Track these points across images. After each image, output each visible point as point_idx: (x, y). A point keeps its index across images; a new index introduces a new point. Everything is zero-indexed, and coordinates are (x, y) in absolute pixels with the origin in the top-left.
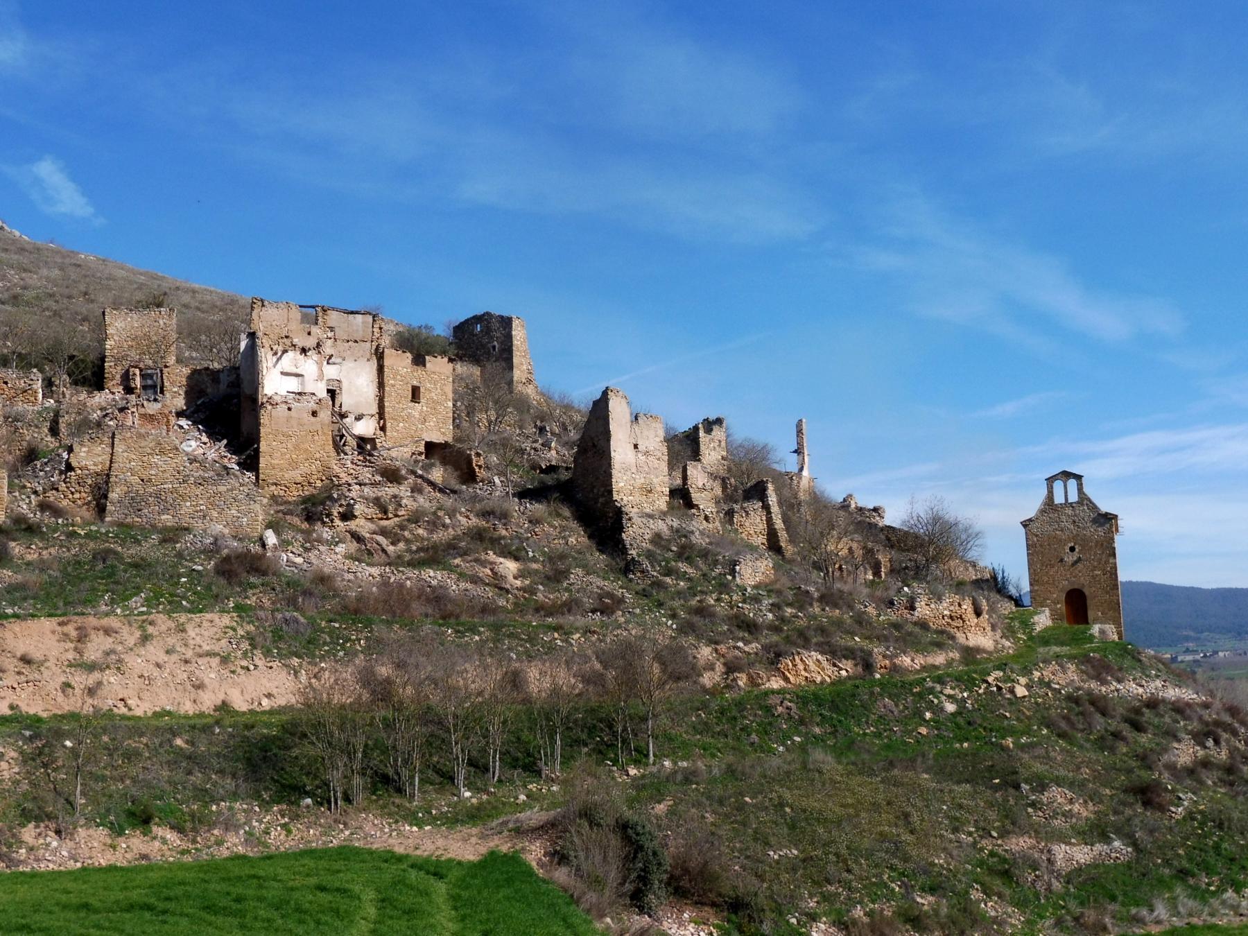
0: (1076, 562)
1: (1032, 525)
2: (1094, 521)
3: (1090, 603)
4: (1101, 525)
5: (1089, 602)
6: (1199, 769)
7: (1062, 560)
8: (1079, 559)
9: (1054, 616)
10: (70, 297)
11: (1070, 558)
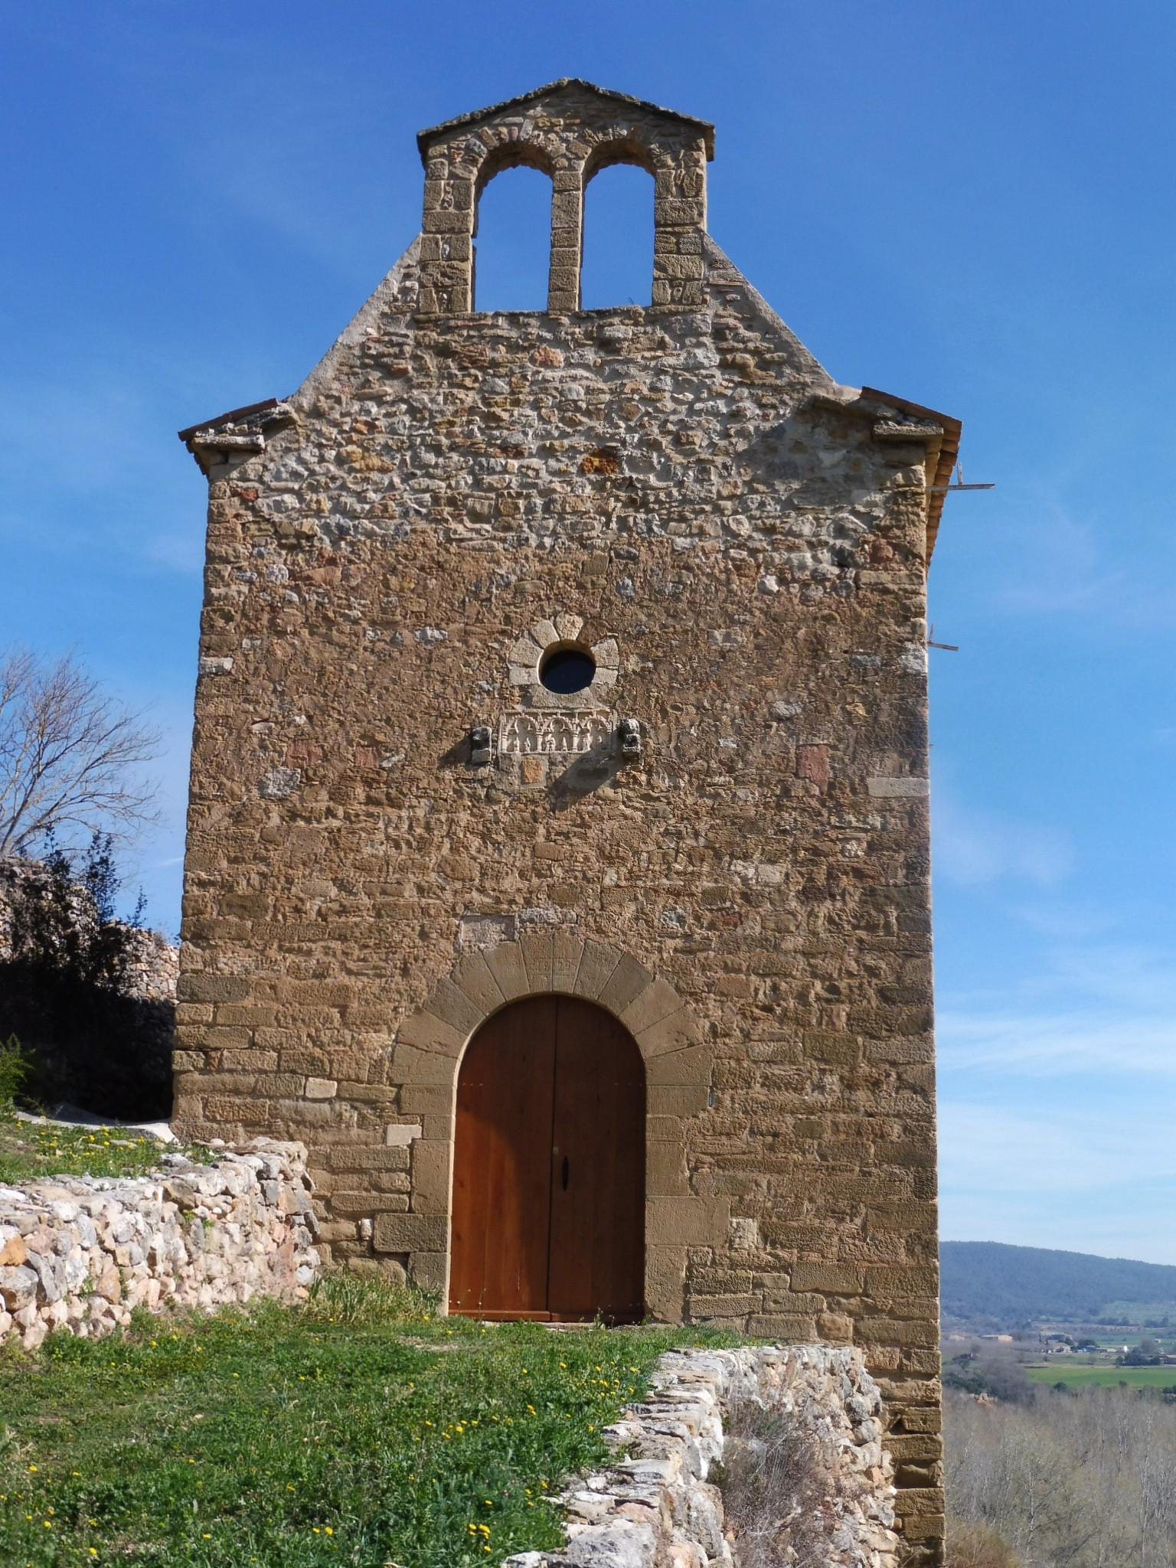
0: (574, 784)
1: (275, 461)
2: (768, 457)
3: (670, 1126)
4: (823, 492)
5: (662, 1117)
6: (848, 1492)
7: (470, 750)
8: (618, 753)
9: (357, 1220)
10: (152, 1260)
11: (542, 740)
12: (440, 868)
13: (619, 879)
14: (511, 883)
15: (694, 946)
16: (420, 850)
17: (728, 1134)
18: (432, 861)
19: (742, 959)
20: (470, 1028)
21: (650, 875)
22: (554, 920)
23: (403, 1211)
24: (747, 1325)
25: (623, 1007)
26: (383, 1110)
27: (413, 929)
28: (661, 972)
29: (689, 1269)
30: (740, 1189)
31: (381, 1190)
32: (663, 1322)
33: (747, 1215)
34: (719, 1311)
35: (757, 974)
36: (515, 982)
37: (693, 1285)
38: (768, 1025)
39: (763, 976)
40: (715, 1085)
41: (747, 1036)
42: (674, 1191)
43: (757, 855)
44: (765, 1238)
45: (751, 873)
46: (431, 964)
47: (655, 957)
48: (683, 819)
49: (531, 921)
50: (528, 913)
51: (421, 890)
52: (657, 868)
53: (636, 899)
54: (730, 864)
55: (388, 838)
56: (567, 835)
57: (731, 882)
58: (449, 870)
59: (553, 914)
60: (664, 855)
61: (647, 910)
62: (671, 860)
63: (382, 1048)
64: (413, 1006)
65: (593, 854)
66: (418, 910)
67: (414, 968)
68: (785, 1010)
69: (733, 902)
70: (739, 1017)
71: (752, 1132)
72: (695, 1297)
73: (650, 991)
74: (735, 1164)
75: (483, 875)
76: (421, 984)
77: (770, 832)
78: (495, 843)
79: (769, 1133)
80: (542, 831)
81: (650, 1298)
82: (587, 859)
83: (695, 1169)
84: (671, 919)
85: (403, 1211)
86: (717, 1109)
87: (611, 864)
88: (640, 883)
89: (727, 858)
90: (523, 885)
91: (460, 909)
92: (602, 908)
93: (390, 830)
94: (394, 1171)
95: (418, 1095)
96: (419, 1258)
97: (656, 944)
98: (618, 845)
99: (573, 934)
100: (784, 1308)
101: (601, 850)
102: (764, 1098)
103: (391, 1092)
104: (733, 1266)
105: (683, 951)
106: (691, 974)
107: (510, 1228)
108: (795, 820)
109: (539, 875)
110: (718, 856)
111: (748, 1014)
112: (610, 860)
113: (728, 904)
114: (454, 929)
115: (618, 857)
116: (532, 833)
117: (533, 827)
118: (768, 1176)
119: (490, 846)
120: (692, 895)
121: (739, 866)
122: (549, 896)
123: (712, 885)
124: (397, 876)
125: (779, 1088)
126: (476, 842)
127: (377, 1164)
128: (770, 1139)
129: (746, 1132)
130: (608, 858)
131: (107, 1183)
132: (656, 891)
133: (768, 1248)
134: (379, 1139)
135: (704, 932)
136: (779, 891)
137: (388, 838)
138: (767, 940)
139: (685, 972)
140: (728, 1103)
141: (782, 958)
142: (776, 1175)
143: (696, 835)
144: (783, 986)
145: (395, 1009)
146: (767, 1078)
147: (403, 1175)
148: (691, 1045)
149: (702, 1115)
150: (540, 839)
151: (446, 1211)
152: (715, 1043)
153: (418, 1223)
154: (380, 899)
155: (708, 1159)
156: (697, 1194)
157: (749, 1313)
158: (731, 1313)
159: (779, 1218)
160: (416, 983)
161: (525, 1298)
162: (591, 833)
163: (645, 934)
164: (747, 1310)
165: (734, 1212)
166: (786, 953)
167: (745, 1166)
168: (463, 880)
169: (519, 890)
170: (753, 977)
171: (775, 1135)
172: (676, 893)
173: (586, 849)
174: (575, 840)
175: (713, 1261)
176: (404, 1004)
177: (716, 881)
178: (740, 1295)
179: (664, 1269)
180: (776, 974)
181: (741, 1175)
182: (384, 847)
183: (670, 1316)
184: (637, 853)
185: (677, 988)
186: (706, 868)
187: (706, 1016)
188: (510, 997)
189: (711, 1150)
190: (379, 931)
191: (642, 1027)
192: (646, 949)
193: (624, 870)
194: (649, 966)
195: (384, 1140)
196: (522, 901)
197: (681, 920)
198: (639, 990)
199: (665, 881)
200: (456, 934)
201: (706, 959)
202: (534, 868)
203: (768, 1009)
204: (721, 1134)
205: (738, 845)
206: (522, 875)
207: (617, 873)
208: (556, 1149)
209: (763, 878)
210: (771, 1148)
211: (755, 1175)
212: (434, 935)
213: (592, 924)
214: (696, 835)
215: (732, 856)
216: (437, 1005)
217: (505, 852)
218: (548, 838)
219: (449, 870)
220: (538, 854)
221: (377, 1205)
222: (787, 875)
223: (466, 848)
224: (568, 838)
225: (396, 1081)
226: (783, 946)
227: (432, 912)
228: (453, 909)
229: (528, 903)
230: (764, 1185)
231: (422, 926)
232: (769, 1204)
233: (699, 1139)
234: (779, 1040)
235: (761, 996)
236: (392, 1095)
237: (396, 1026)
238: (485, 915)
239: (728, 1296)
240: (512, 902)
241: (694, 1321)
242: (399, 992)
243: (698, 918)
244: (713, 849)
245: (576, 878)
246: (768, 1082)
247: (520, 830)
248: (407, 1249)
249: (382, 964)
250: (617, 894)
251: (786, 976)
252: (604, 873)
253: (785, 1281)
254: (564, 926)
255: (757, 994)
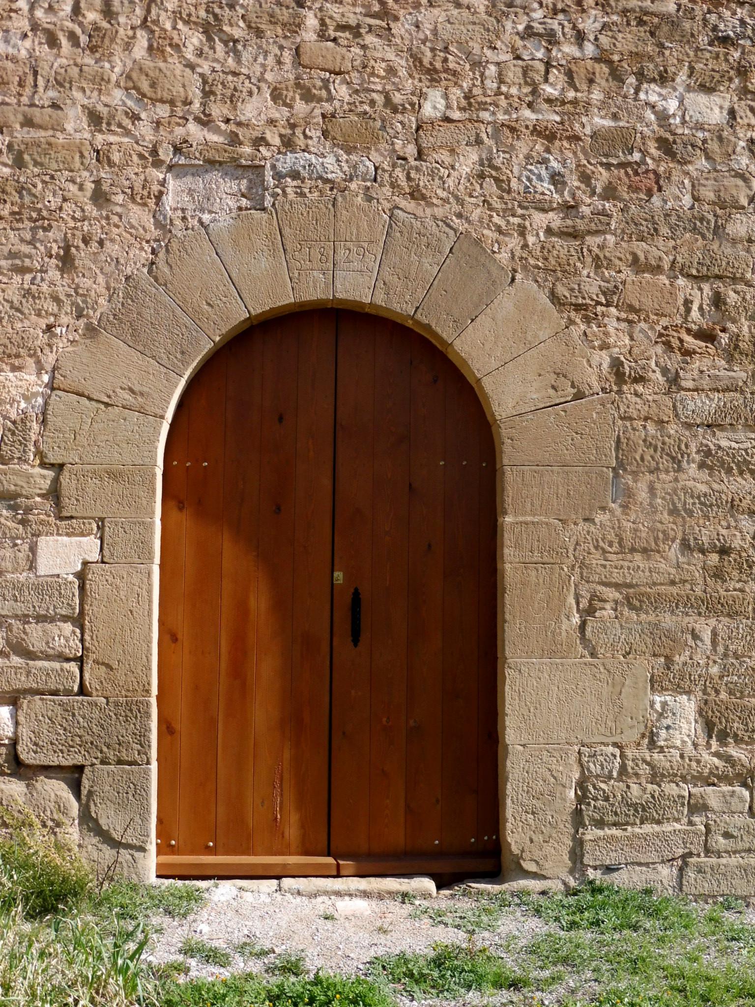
12: (129, 83)
13: (448, 107)
14: (255, 109)
15: (581, 225)
16: (93, 49)
17: (645, 551)
18: (116, 68)
19: (655, 250)
20: (185, 364)
21: (503, 102)
22: (336, 175)
23: (68, 693)
24: (681, 876)
25: (460, 328)
26: (28, 510)
27: (81, 188)
28: (525, 268)
29: (581, 784)
30: (665, 647)
31: (29, 655)
32: (535, 876)
33: (679, 690)
34: (634, 856)
35: (689, 276)
36: (268, 283)
37: (588, 813)
38: (707, 364)
39: (698, 279)
40: (621, 464)
41: (674, 381)
42: (553, 650)
43: (682, 77)
44: (709, 727)
45: (672, 105)
46: (113, 249)
47: (514, 242)
48: (555, 12)
49: (295, 175)
50: (287, 162)
51: (95, 119)
52: (514, 91)
53: (479, 142)
54: (637, 90)
55: (35, 27)
56: (356, 31)
57: (641, 118)
58: (144, 88)
59: (332, 165)
60: (525, 71)
61: (498, 162)
62: (538, 78)
63: (26, 398)
64: (82, 322)
65: (401, 64)
66: (90, 158)
67: (82, 256)
68: (736, 339)
69: (644, 153)
70: (659, 349)
71: (685, 546)
72: (591, 834)
73: (506, 302)
74: (657, 602)
75: (207, 94)
76: (94, 284)
77: (703, 40)
78: (231, 42)
79: (713, 549)
80: (312, 21)
81: (516, 835)
82: (391, 71)
83: (590, 611)
84: (540, 178)
85: (68, 693)
86: (625, 507)
87: (434, 81)
88: (485, 116)
89: (632, 80)
90: (280, 114)
91: (166, 154)
92: (420, 156)
93: (39, 13)
94: (52, 620)
95: (92, 484)
96: (101, 778)
97: (516, 220)
98: (446, 49)
99: (369, 199)
100: (740, 846)
101: (417, 59)
102: (703, 488)
103: (43, 478)
104: (656, 777)
105: (563, 234)
106: (576, 273)
107: (263, 712)
108: (743, 22)
109: (308, 97)
110: (616, 75)
111: (675, 343)
112: (432, 75)
113: (637, 156)
114: (155, 188)
115: (447, 70)
116: (295, 26)
117: (297, 15)
118: (713, 622)
119: (219, 47)
120: (576, 138)
121: (652, 93)
122: (325, 134)
123: (608, 123)
124: (51, 93)
125: (729, 471)
126: (195, 39)
127: (20, 608)
128: (714, 558)
129: (676, 545)
130: (428, 71)
131: (496, 414)
132: (513, 130)
133: (714, 743)
134: (23, 563)
135: (599, 204)
136: (720, 138)
137: (35, 27)
138: (702, 220)
139: (567, 271)
140: (643, 495)
141: (728, 251)
142: (725, 620)
143: (580, 37)
144: (732, 298)
145: (49, 328)
146: (708, 453)
147: (68, 627)
148: (579, 396)
149: (599, 517)
150: (309, 35)
151: (148, 692)
152: (620, 392)
153: (96, 714)
154: (21, 134)
155: (612, 594)
156: (593, 655)
157: (684, 857)
158: (653, 857)
159: (731, 693)
160: (85, 283)
161: (292, 832)
162: (396, 29)
163: (497, 204)
164: (680, 852)
165: (656, 684)
166: (734, 242)
167: (676, 604)
168: (172, 103)
169: (272, 122)
170: (681, 281)
171: (724, 551)
172: (549, 136)
173: (391, 55)
174: (370, 39)
175: (623, 769)
176: (65, 319)
177: (615, 117)
178: (667, 827)
179: (539, 786)
180: (719, 277)
181: (668, 621)
182: (28, 43)
183: (549, 868)
184: (478, 64)
185: (553, 296)
186: (597, 96)
187: (604, 346)
188: (257, 309)
189: (617, 578)
190: (20, 190)
191: (494, 364)
192: (499, 230)
193: (456, 93)
194: (503, 257)
195: (32, 566)
196: (277, 141)
197: (557, 179)
198: (486, 299)
199: (527, 113)
200: (159, 197)
201: (601, 247)
202: (298, 85)
203: (707, 336)
204: (633, 550)
205: (651, 59)
206: (276, 95)
207: (446, 97)
208: (339, 576)
209: (693, 114)
210: (718, 574)
211: (691, 621)
212: (119, 199)
213: (403, 183)
214: (580, 37)
215: (641, 76)
216: (126, 321)
217: (246, 56)
218: (322, 35)
219: (144, 88)
220: (305, 60)
221: (22, 682)
222: (732, 113)
223: (177, 47)
224: (358, 35)
225: (52, 458)
226: (730, 229)
227: (116, 157)
228: (154, 152)
229: (288, 144)
230: (707, 637)
231: (98, 182)
232: (715, 670)
233: (596, 559)
234: (727, 390)
235: (695, 314)
236: (46, 484)
237: (49, 359)
238: (211, 163)
239: (648, 828)
240: (260, 141)
241: (591, 874)
242: (56, 299)
243: (586, 178)
244: (609, 62)
245: (372, 103)
246: (710, 461)
247: (273, 20)
248: (79, 760)
249: (26, 249)
250: (445, 133)
251: (734, 279)
252: (422, 95)
253: (742, 799)
254: (353, 186)
255: (688, 310)
